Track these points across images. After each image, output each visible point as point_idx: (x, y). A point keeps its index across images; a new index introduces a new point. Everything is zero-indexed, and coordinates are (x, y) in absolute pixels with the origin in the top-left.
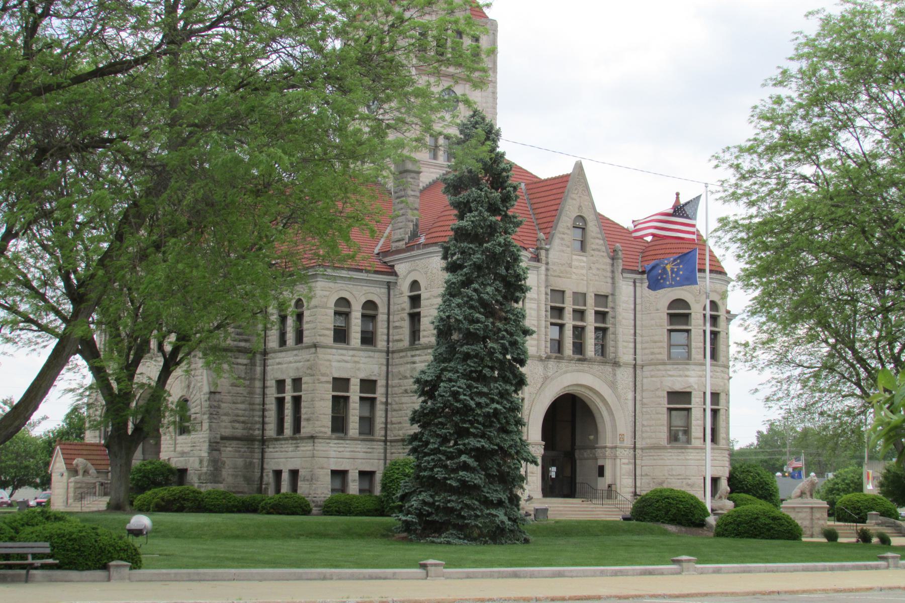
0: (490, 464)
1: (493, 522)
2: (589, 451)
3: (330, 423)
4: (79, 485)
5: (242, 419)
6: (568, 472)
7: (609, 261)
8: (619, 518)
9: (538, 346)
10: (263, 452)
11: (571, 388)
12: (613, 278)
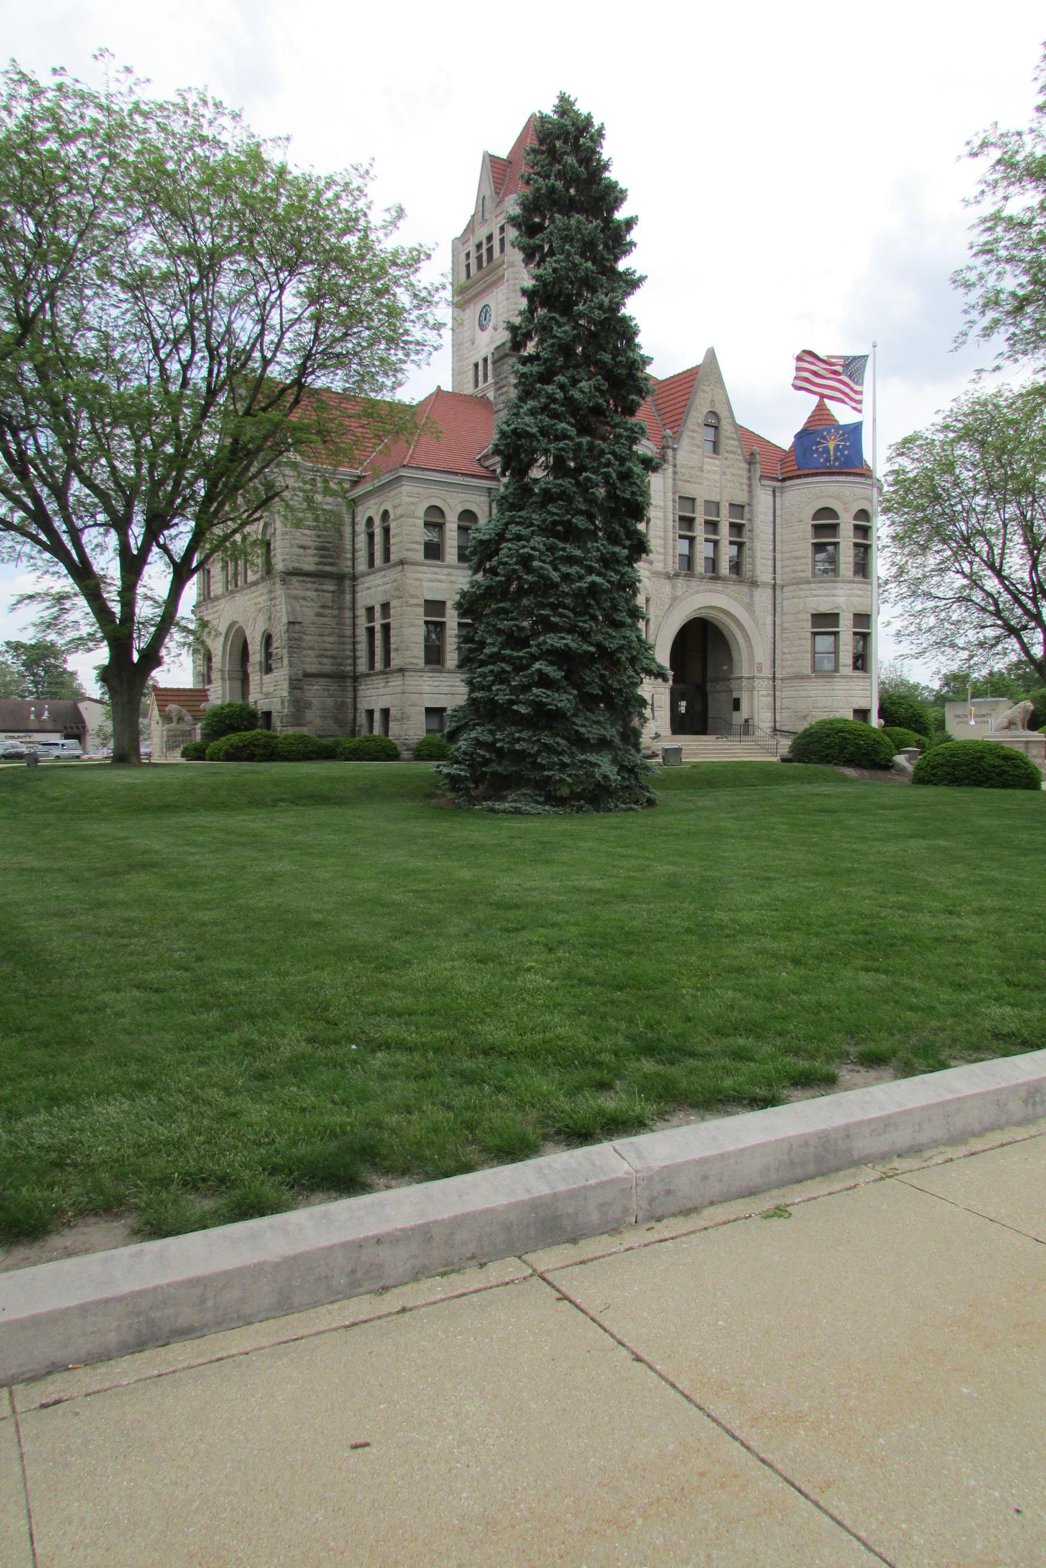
0: (587, 675)
1: (590, 775)
2: (722, 683)
3: (423, 653)
4: (172, 733)
5: (330, 653)
6: (698, 707)
7: (745, 466)
8: (775, 759)
9: (665, 561)
11: (703, 611)
12: (750, 486)
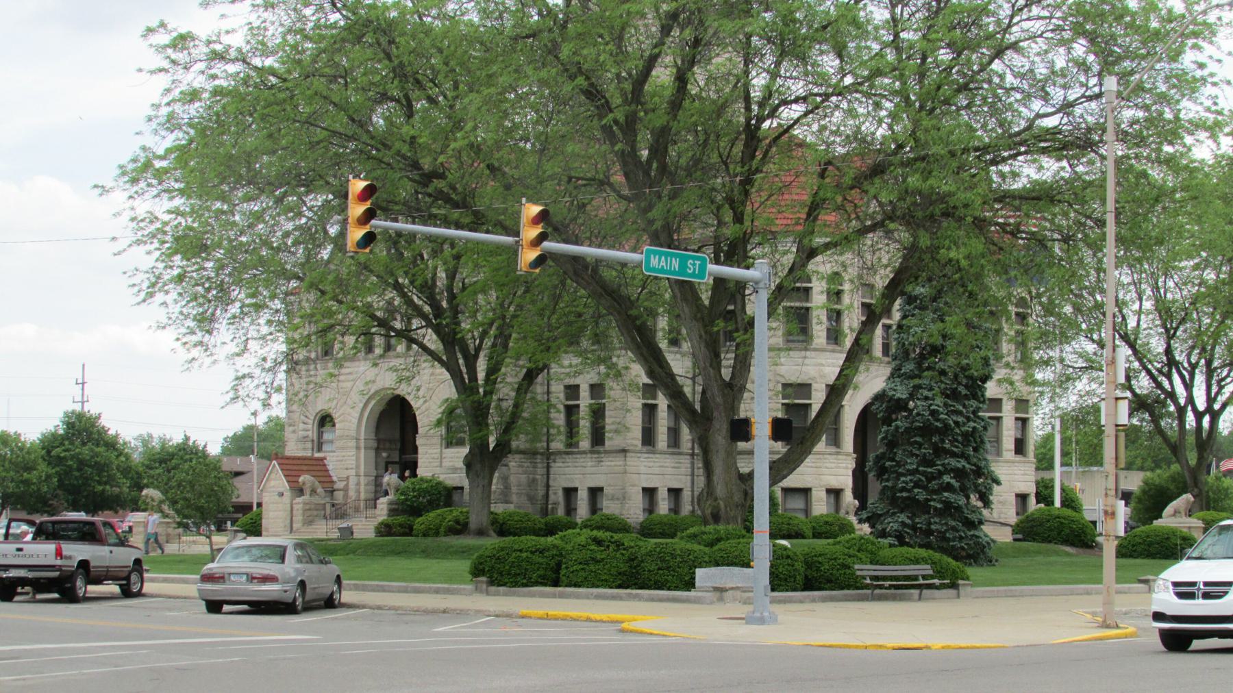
4: (307, 507)
10: (548, 467)
